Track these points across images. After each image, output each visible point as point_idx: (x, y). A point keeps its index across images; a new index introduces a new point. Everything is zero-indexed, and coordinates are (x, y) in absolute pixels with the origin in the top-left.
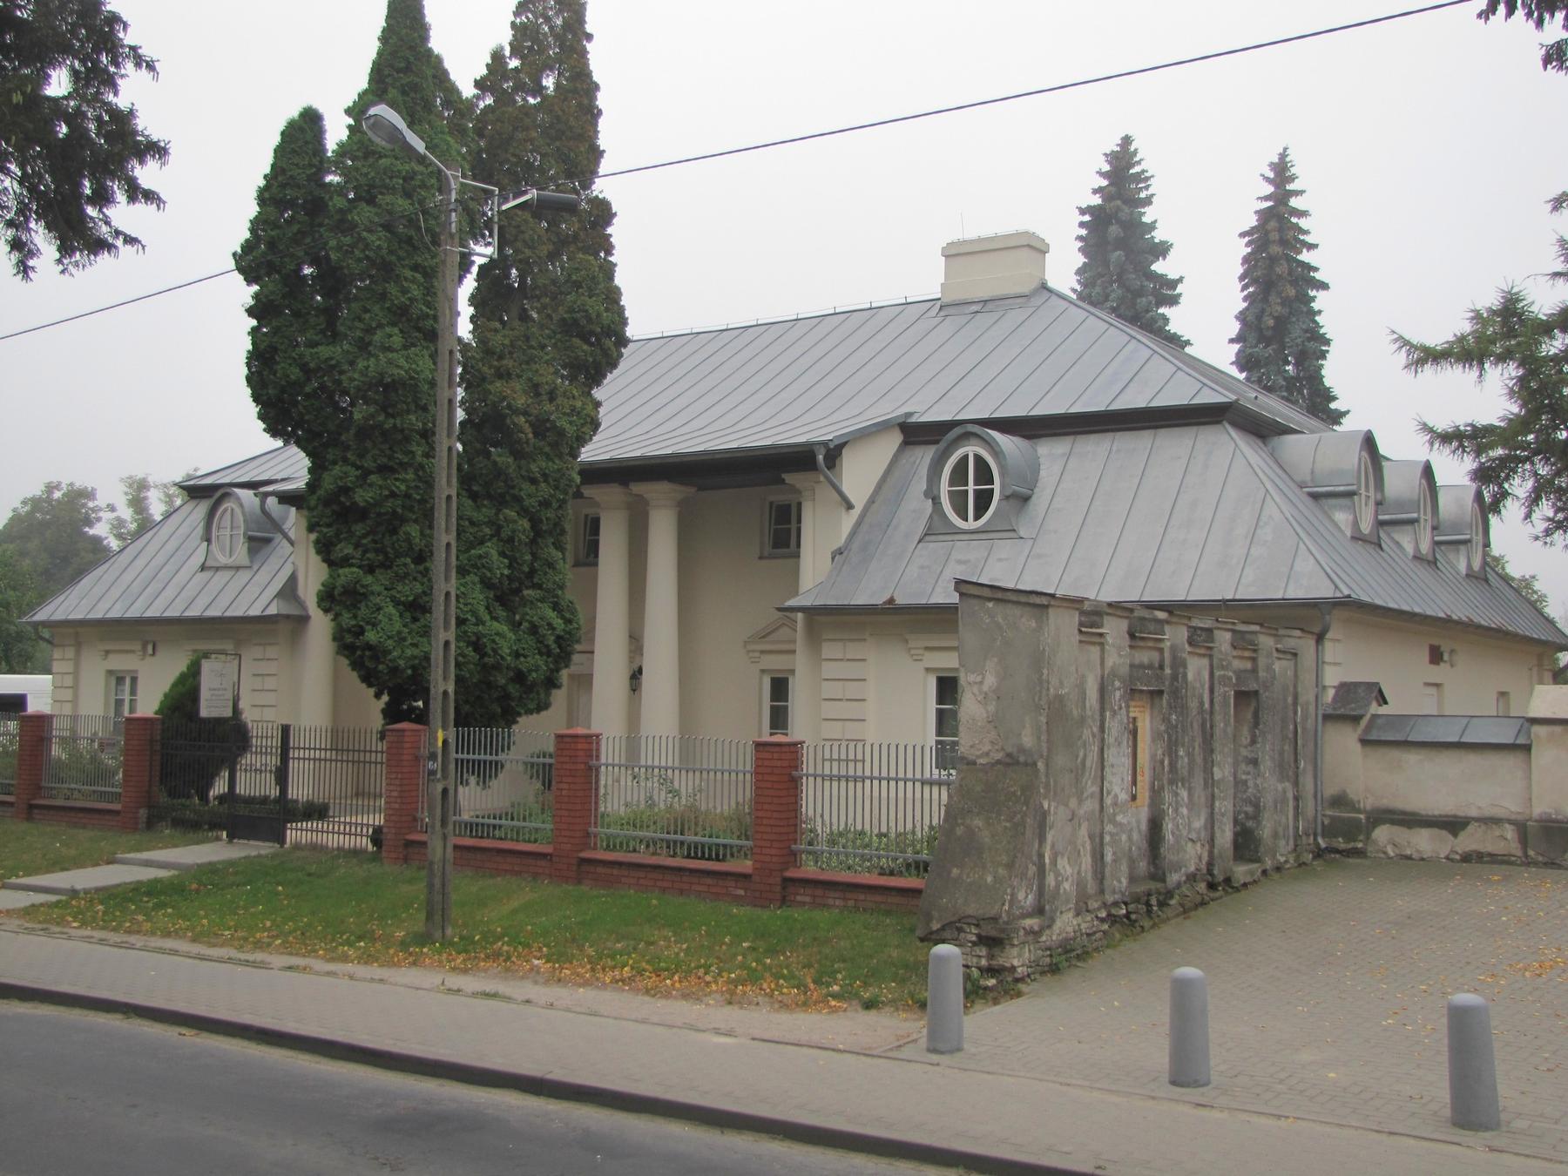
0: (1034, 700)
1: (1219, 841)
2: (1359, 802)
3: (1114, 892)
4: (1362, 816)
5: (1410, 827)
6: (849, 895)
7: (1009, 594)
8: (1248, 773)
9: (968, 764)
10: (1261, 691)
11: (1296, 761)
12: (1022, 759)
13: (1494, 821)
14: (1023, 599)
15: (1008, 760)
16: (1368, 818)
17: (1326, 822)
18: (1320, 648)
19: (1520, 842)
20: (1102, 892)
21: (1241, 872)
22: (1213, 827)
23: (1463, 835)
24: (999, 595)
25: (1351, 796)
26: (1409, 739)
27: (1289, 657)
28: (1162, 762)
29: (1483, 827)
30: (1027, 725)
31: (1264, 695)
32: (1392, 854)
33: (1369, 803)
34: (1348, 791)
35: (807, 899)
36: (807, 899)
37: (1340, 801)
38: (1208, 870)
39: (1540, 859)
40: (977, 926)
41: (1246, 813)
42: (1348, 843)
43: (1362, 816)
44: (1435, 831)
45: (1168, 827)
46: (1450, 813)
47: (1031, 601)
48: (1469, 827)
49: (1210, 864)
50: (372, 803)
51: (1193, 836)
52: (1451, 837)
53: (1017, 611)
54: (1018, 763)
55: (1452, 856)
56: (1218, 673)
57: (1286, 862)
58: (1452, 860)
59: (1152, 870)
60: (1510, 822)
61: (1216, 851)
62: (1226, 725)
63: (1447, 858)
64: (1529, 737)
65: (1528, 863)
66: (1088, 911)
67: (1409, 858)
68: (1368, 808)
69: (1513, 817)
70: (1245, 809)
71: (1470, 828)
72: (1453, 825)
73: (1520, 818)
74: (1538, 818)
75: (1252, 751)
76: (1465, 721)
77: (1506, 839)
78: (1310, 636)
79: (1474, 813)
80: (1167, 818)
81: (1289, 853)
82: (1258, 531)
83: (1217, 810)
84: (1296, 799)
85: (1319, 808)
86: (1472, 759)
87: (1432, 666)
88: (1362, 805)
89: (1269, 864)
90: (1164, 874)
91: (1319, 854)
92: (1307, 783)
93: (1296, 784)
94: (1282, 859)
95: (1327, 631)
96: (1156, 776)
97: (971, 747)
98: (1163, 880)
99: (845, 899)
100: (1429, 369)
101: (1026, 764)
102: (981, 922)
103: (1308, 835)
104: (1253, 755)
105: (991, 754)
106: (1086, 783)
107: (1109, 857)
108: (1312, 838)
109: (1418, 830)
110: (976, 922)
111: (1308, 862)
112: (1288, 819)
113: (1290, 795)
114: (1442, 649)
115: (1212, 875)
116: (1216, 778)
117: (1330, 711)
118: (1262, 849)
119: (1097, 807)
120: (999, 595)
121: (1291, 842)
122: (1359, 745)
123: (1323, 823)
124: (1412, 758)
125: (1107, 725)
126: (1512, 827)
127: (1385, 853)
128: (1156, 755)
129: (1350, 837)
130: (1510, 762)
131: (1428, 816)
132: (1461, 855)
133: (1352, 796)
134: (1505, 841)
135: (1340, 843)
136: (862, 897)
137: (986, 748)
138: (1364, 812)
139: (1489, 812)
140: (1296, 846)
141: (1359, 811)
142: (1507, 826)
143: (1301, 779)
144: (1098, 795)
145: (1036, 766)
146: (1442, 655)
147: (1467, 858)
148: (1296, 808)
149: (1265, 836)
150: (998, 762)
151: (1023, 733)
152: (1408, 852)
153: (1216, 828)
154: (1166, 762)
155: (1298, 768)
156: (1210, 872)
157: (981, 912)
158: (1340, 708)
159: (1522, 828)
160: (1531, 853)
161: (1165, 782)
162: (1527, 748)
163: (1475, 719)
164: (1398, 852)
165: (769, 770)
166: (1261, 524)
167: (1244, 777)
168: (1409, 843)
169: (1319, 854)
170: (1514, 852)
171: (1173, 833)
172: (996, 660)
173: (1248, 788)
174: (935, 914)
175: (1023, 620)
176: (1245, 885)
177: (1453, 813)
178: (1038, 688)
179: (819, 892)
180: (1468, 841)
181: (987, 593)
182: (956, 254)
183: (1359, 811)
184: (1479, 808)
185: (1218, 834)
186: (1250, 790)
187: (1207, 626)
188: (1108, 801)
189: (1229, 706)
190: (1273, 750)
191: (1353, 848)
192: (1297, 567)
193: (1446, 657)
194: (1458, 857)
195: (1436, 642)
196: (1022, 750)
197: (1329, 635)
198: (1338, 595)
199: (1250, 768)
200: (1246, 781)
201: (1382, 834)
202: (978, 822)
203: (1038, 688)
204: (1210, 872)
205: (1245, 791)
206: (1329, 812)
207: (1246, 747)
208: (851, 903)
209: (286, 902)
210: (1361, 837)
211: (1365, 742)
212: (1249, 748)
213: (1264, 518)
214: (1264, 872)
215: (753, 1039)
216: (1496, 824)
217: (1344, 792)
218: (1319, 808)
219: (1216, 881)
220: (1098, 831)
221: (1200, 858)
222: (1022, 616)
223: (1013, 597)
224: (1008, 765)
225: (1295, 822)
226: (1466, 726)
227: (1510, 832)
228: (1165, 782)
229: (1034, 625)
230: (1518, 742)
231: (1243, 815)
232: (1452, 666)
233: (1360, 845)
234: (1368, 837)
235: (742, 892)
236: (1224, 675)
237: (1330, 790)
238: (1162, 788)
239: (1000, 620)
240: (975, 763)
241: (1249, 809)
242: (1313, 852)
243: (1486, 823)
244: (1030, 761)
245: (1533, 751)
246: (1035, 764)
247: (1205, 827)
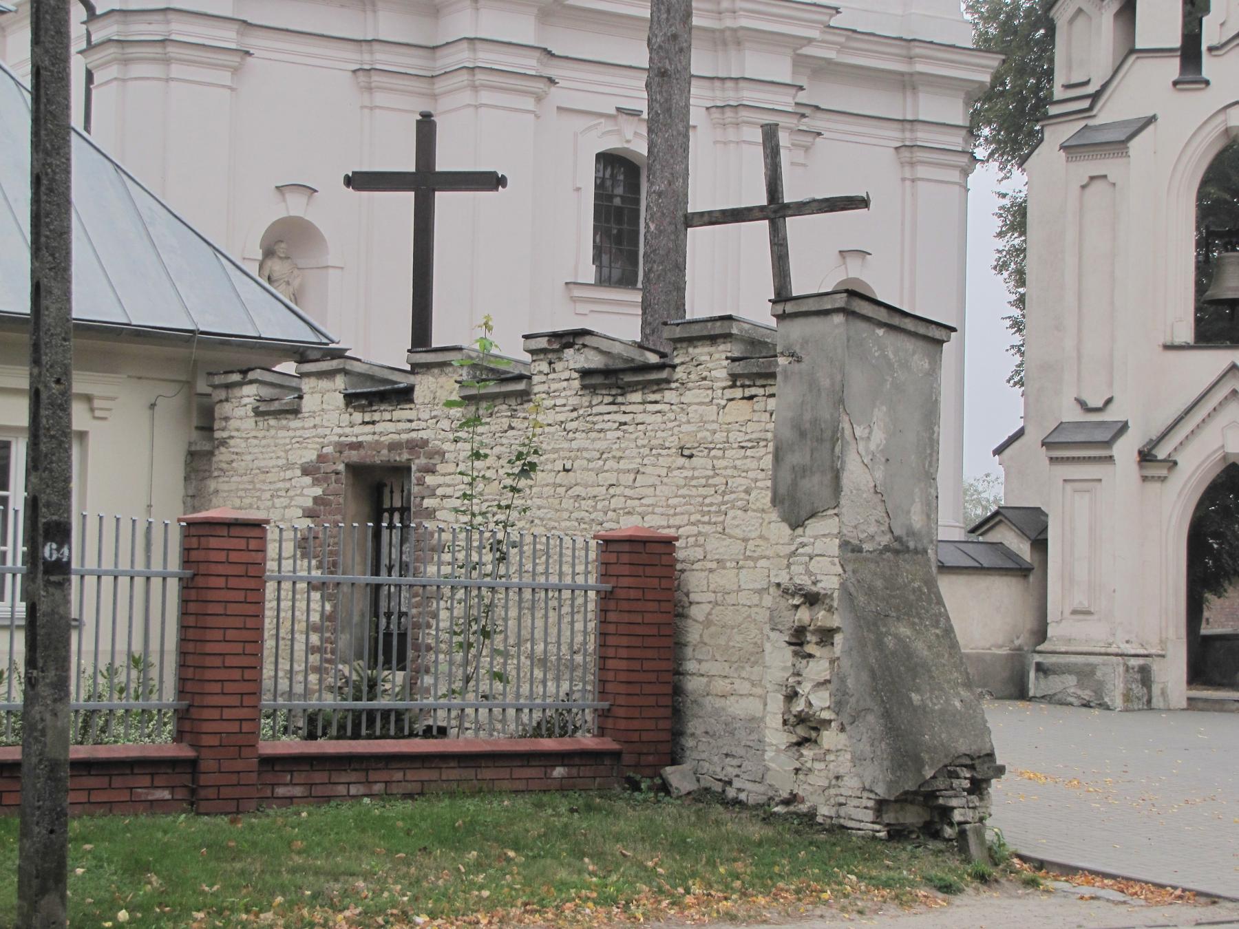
0: (924, 467)
3: (1111, 700)
6: (373, 776)
7: (907, 320)
9: (853, 551)
12: (911, 545)
14: (922, 329)
15: (896, 545)
24: (896, 321)
30: (917, 500)
35: (298, 791)
36: (298, 791)
40: (972, 767)
47: (930, 334)
50: (552, 649)
53: (909, 344)
54: (907, 550)
76: (637, 484)
97: (855, 527)
99: (368, 783)
101: (916, 551)
102: (977, 762)
110: (969, 762)
120: (896, 321)
136: (398, 776)
137: (872, 529)
145: (927, 552)
150: (887, 548)
151: (913, 510)
157: (974, 747)
165: (240, 570)
172: (884, 408)
174: (925, 756)
175: (916, 357)
178: (928, 451)
179: (319, 777)
181: (882, 315)
196: (911, 533)
202: (904, 630)
203: (928, 451)
208: (378, 788)
209: (413, 870)
215: (1198, 924)
222: (914, 353)
223: (909, 324)
224: (897, 552)
229: (927, 366)
235: (166, 795)
239: (891, 356)
240: (860, 550)
244: (920, 547)
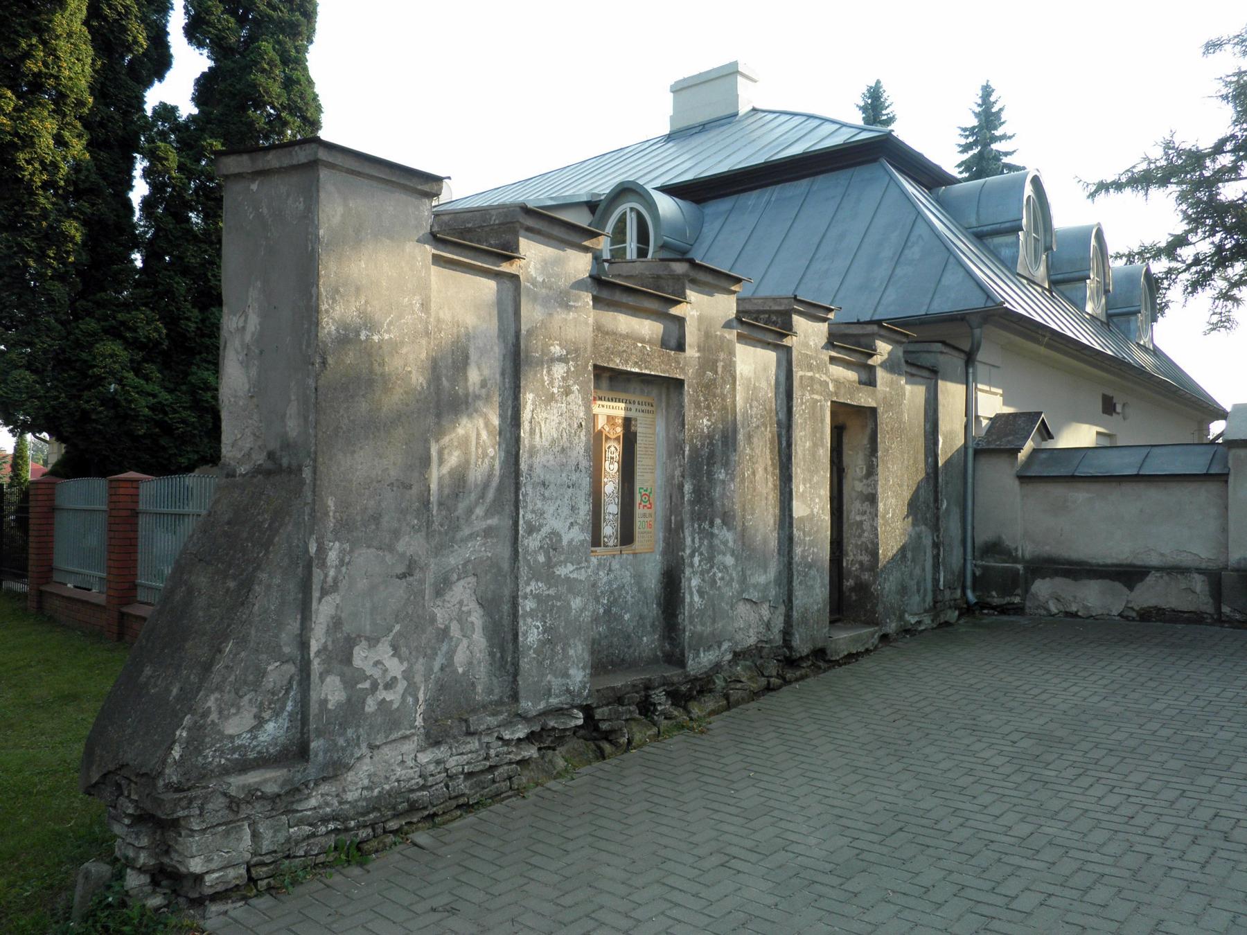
1: (801, 598)
2: (1016, 549)
4: (1020, 566)
5: (1075, 579)
8: (864, 513)
10: (880, 410)
11: (936, 500)
13: (1175, 571)
16: (1026, 568)
17: (978, 573)
18: (971, 370)
19: (1212, 596)
20: (515, 697)
21: (844, 639)
22: (790, 582)
23: (1140, 588)
25: (1007, 543)
26: (1076, 474)
27: (926, 373)
28: (681, 487)
29: (1166, 578)
31: (884, 418)
32: (1054, 610)
33: (1027, 550)
34: (1004, 537)
37: (994, 548)
38: (785, 640)
39: (1238, 616)
41: (861, 563)
42: (1003, 597)
43: (1020, 566)
44: (1107, 583)
45: (692, 582)
46: (1125, 562)
48: (1148, 579)
49: (787, 633)
51: (754, 595)
52: (1125, 590)
55: (1125, 614)
56: (798, 373)
57: (919, 622)
58: (1127, 618)
59: (668, 647)
60: (1200, 571)
61: (795, 614)
62: (815, 445)
63: (1120, 615)
64: (1226, 465)
65: (1220, 620)
66: (469, 733)
67: (1074, 615)
68: (1027, 556)
69: (1203, 565)
70: (860, 558)
71: (1150, 579)
72: (1130, 575)
73: (1212, 566)
74: (1235, 566)
75: (868, 485)
77: (1195, 592)
78: (956, 353)
79: (1154, 560)
80: (688, 571)
81: (926, 611)
82: (906, 252)
83: (797, 559)
84: (936, 545)
85: (969, 557)
86: (1154, 495)
87: (1106, 416)
88: (1020, 553)
89: (892, 627)
90: (683, 654)
91: (968, 610)
92: (953, 527)
93: (936, 528)
94: (913, 620)
95: (978, 349)
96: (674, 507)
98: (681, 663)
100: (1102, 196)
103: (952, 588)
104: (870, 490)
105: (254, 456)
106: (470, 511)
107: (532, 634)
108: (959, 592)
109: (1086, 582)
111: (953, 621)
112: (924, 570)
113: (927, 541)
114: (1115, 401)
115: (790, 648)
116: (795, 515)
117: (983, 445)
118: (880, 608)
119: (506, 552)
121: (929, 598)
122: (1017, 483)
123: (974, 574)
124: (1080, 496)
125: (526, 415)
126: (1202, 577)
127: (1048, 610)
128: (673, 477)
129: (1006, 590)
130: (1203, 494)
131: (1099, 565)
132: (1137, 612)
133: (1008, 542)
134: (1194, 594)
135: (996, 599)
138: (1023, 560)
139: (1172, 559)
140: (935, 602)
141: (1016, 560)
142: (1196, 576)
143: (942, 524)
144: (507, 532)
146: (1115, 405)
147: (1146, 615)
148: (936, 557)
149: (886, 592)
152: (1074, 608)
153: (795, 583)
154: (688, 487)
155: (938, 509)
156: (787, 643)
158: (995, 441)
159: (1215, 578)
160: (1226, 609)
161: (687, 517)
162: (1223, 478)
163: (1156, 448)
164: (1062, 608)
166: (909, 244)
167: (858, 518)
168: (1075, 597)
169: (968, 610)
170: (1204, 608)
171: (701, 593)
172: (259, 284)
173: (863, 531)
176: (851, 657)
177: (1129, 561)
180: (1147, 595)
182: (680, 89)
183: (1016, 560)
184: (1162, 555)
185: (799, 592)
186: (866, 534)
187: (782, 308)
188: (531, 543)
189: (823, 421)
190: (901, 486)
191: (1009, 604)
192: (945, 281)
193: (1119, 408)
194: (1134, 614)
195: (1109, 393)
197: (980, 356)
198: (990, 304)
199: (867, 504)
200: (861, 522)
201: (1042, 588)
204: (787, 643)
205: (860, 536)
206: (979, 562)
207: (861, 481)
210: (1019, 591)
211: (1023, 479)
212: (865, 481)
213: (913, 239)
214: (885, 638)
216: (1182, 573)
217: (1000, 537)
218: (969, 557)
219: (796, 655)
220: (507, 592)
221: (768, 626)
224: (269, 473)
225: (934, 574)
226: (1147, 456)
227: (1199, 584)
228: (687, 517)
230: (1212, 471)
231: (857, 566)
232: (1124, 419)
233: (1017, 600)
234: (1027, 591)
236: (812, 378)
237: (984, 535)
238: (680, 526)
241: (865, 558)
242: (960, 609)
243: (1168, 574)
245: (1231, 479)
246: (300, 469)
247: (778, 582)
